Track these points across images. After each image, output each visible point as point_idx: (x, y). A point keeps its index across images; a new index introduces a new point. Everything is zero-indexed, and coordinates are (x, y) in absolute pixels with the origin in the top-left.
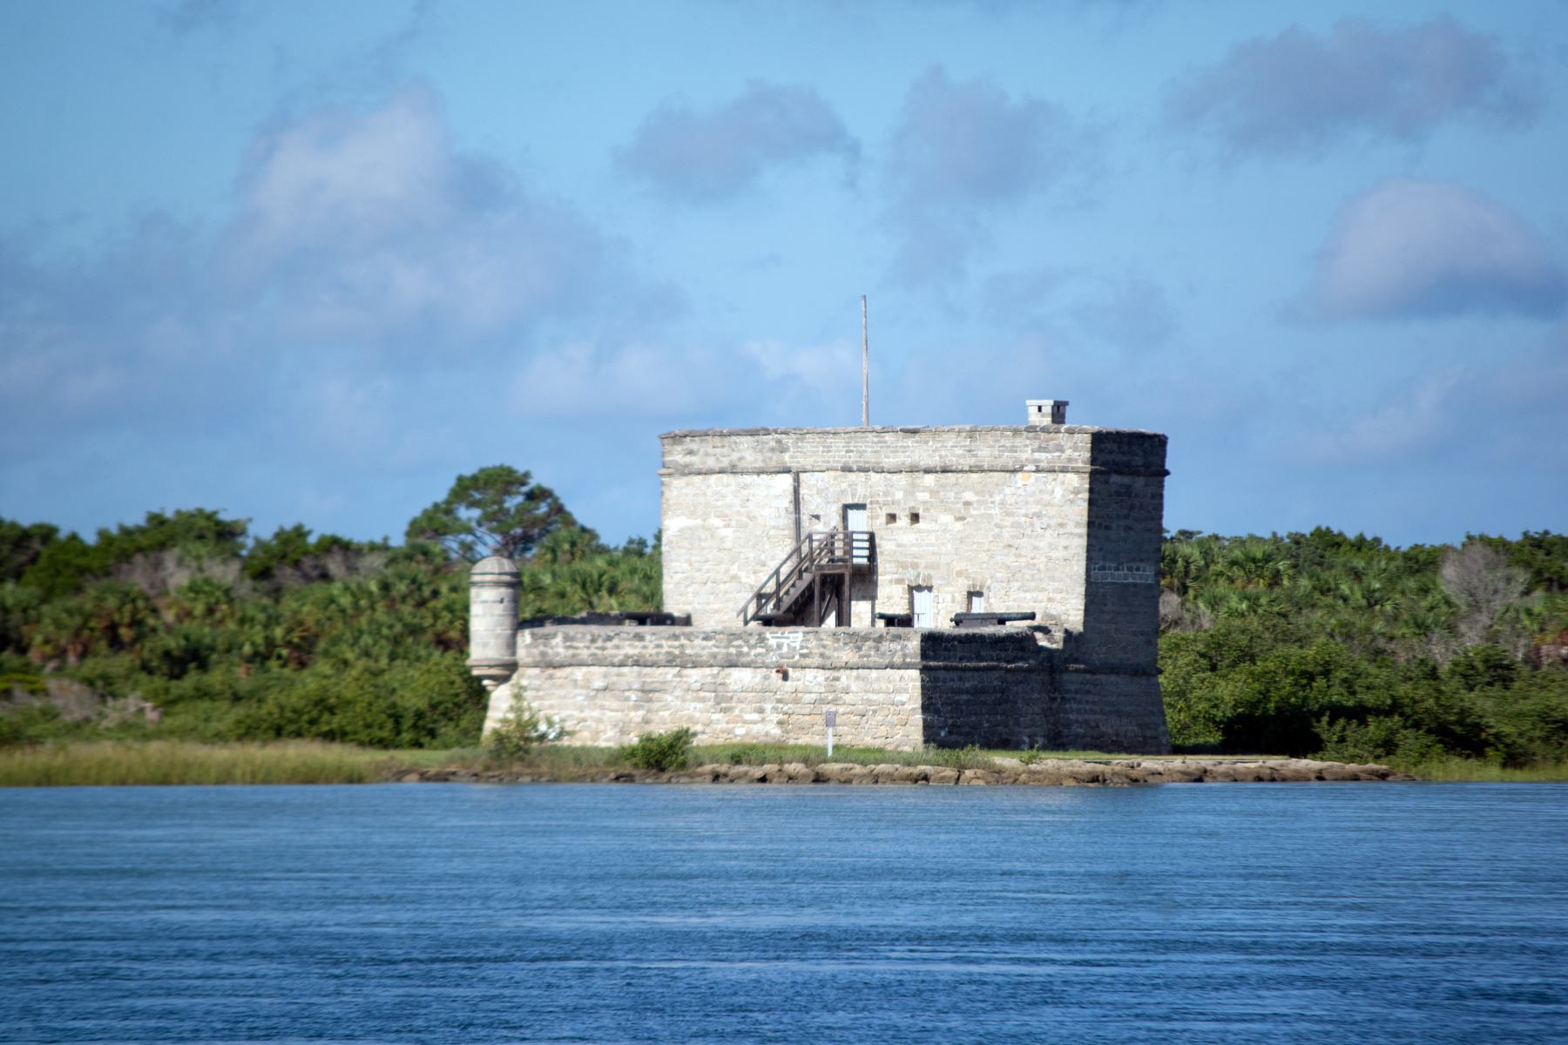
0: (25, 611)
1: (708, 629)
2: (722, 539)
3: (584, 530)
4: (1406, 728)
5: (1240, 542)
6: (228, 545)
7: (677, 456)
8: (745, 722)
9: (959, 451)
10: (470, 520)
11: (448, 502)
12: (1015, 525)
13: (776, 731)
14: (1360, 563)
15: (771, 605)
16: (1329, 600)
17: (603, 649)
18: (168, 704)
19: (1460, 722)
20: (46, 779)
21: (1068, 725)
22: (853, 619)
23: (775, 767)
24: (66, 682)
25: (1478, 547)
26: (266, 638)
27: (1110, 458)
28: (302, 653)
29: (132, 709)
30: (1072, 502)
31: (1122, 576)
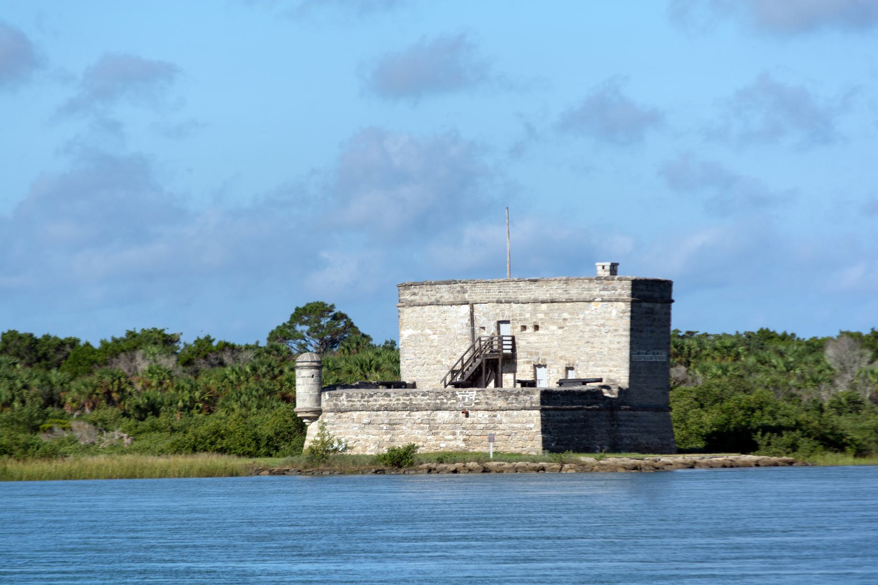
0: (62, 384)
1: (425, 390)
2: (432, 341)
3: (364, 336)
4: (803, 437)
5: (718, 337)
6: (170, 347)
7: (407, 296)
8: (446, 440)
9: (560, 291)
10: (302, 331)
11: (290, 322)
12: (591, 331)
13: (463, 445)
14: (782, 347)
15: (459, 377)
16: (766, 367)
17: (368, 402)
18: (136, 435)
19: (832, 434)
20: (69, 476)
21: (621, 439)
22: (504, 383)
23: (462, 464)
24: (82, 423)
25: (845, 337)
26: (191, 397)
27: (642, 293)
28: (210, 405)
29: (117, 437)
30: (621, 317)
31: (649, 357)
